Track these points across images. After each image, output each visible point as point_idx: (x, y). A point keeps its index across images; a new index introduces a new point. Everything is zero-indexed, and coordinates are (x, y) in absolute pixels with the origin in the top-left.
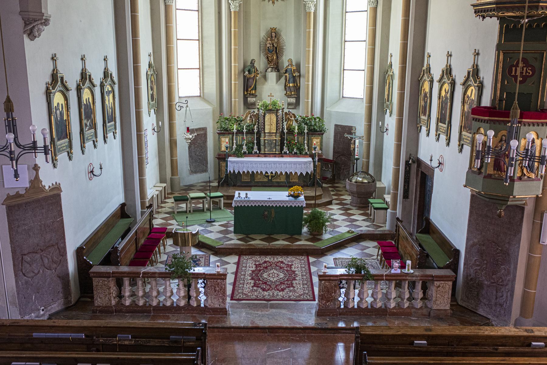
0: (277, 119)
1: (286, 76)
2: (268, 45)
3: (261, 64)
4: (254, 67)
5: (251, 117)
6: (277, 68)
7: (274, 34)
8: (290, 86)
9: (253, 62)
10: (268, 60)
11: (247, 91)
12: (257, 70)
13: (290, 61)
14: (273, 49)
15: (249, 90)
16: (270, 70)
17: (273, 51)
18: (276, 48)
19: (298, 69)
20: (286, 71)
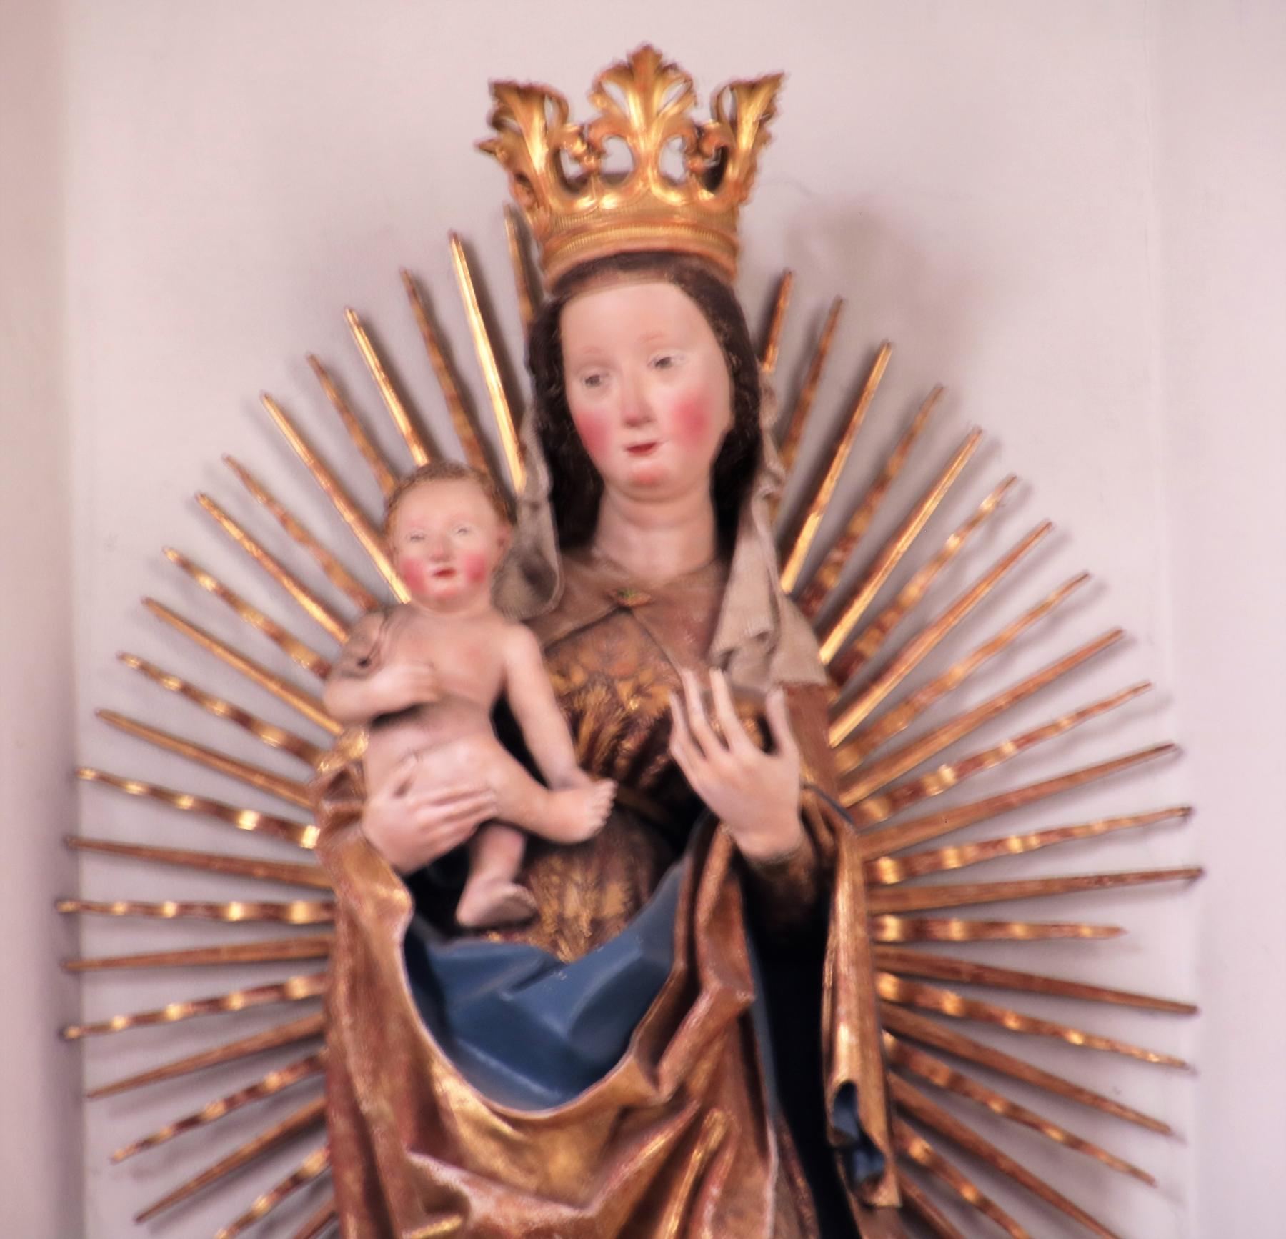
2: (433, 785)
7: (647, 373)
17: (646, 1003)
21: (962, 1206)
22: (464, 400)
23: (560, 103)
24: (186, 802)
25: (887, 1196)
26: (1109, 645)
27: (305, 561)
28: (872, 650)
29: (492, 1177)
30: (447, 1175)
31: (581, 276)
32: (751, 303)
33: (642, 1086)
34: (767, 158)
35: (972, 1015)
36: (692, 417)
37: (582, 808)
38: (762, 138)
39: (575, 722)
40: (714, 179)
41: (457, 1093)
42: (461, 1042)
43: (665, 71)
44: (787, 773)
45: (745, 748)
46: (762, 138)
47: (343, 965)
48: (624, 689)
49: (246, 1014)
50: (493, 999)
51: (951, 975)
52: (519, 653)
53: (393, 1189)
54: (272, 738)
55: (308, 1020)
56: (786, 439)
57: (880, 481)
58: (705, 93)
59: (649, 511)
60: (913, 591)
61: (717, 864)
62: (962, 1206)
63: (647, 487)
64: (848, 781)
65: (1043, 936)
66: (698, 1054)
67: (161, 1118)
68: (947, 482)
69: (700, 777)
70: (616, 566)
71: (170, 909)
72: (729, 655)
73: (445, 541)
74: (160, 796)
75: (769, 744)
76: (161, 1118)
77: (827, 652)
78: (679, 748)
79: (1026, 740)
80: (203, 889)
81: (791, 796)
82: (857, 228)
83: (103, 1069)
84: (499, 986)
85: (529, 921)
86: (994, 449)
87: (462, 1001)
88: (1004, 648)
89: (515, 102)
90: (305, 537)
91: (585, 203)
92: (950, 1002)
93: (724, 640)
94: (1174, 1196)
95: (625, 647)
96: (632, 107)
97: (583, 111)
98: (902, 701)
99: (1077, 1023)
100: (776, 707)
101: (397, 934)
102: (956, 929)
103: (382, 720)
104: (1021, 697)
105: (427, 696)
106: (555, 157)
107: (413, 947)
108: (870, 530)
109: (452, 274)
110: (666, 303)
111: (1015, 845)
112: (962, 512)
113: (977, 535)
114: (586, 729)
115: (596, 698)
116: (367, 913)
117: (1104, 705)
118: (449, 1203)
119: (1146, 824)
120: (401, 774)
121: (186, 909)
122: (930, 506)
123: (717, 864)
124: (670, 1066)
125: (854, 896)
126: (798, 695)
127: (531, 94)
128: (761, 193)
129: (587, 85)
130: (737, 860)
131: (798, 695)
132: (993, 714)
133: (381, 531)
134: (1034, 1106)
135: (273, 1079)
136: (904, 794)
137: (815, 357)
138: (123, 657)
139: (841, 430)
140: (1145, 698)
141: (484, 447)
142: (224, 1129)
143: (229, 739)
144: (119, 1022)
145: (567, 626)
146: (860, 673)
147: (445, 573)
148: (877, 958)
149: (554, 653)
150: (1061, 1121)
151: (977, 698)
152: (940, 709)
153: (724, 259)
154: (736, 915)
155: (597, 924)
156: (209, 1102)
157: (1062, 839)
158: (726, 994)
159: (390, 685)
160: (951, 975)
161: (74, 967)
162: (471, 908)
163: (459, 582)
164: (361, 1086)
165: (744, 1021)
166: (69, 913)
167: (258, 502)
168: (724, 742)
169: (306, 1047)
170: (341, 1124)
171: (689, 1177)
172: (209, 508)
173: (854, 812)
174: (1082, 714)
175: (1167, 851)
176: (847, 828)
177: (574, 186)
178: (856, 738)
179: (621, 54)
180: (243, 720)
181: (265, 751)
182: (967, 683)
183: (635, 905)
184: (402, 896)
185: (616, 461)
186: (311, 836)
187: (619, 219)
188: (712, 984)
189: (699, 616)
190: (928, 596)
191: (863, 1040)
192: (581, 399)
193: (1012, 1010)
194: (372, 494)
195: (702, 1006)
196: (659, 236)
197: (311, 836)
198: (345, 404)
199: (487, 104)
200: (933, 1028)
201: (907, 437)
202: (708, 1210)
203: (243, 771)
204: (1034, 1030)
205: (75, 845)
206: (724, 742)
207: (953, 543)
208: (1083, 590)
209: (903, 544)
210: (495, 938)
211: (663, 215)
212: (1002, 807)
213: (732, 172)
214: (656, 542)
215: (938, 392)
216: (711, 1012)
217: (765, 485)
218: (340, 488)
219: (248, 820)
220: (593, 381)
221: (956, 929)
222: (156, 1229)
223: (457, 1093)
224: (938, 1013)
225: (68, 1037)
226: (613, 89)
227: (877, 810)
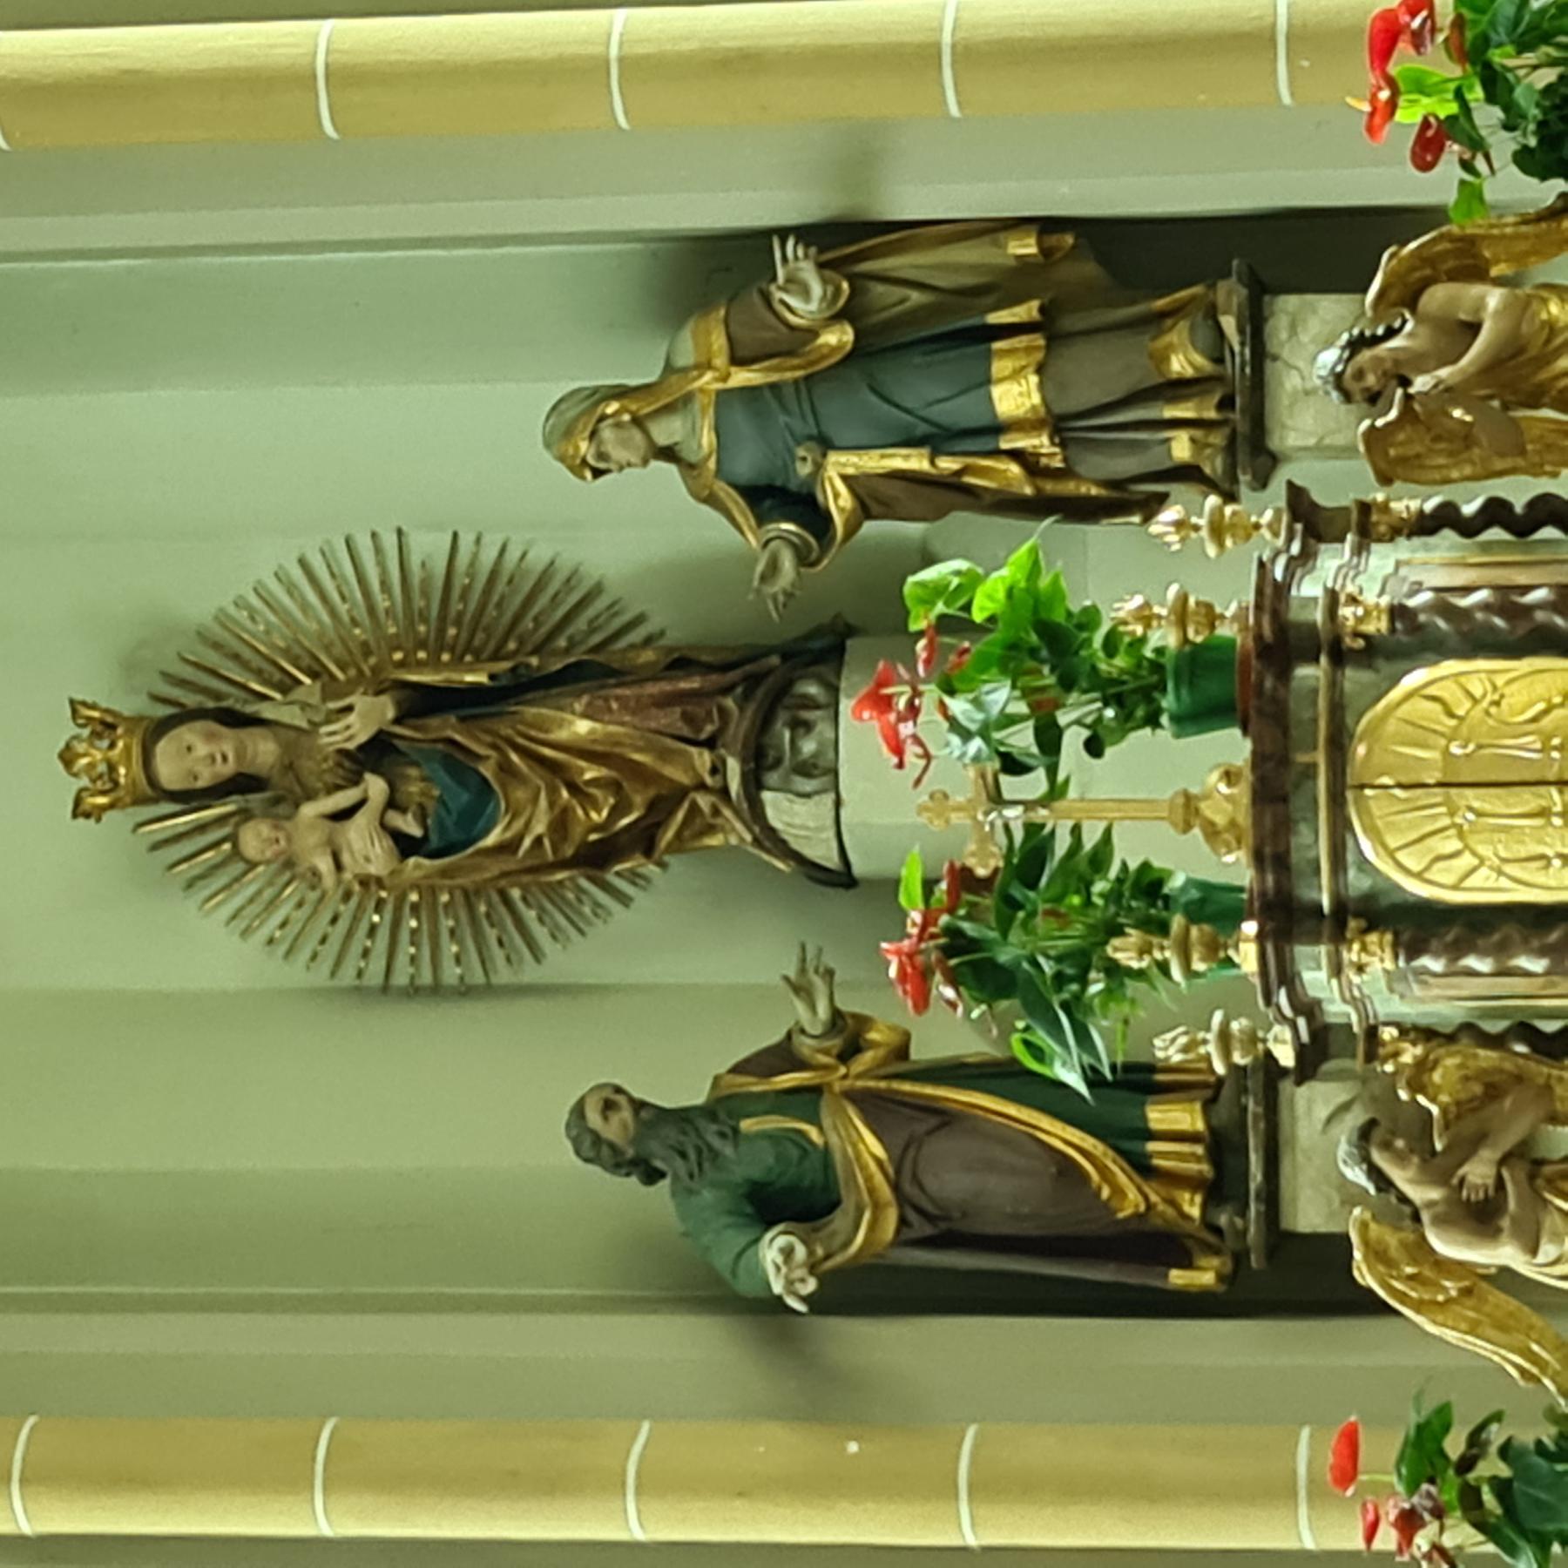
0: (1475, 641)
1: (873, 498)
2: (366, 847)
3: (680, 985)
4: (723, 1108)
5: (1481, 1216)
6: (763, 685)
7: (191, 756)
8: (1058, 424)
9: (636, 1140)
10: (644, 840)
11: (1171, 1246)
12: (782, 1056)
13: (588, 429)
14: (457, 752)
15: (1132, 1198)
16: (793, 814)
17: (457, 762)
18: (420, 703)
19: (718, 270)
20: (779, 497)
21: (536, 629)
22: (201, 828)
23: (81, 790)
24: (369, 943)
25: (534, 661)
26: (303, 563)
27: (268, 893)
28: (306, 661)
29: (527, 825)
30: (527, 842)
31: (152, 781)
32: (163, 711)
33: (492, 763)
34: (104, 705)
35: (458, 622)
36: (210, 737)
37: (375, 786)
38: (93, 707)
39: (338, 788)
40: (112, 727)
41: (491, 840)
42: (475, 832)
43: (68, 747)
44: (358, 700)
45: (352, 718)
46: (93, 707)
47: (438, 882)
48: (325, 766)
49: (457, 920)
50: (456, 824)
51: (441, 631)
52: (309, 810)
53: (529, 863)
54: (342, 908)
55: (458, 893)
56: (218, 696)
57: (236, 657)
58: (78, 731)
59: (249, 756)
60: (282, 644)
61: (398, 730)
62: (536, 629)
63: (240, 756)
64: (360, 672)
65: (425, 594)
66: (478, 741)
67: (498, 955)
68: (238, 630)
69: (362, 738)
70: (272, 767)
71: (412, 950)
72: (310, 722)
73: (264, 841)
74: (366, 953)
75: (349, 709)
76: (498, 955)
77: (307, 680)
78: (351, 746)
79: (343, 598)
80: (404, 936)
81: (369, 699)
82: (130, 666)
83: (478, 977)
84: (449, 822)
85: (422, 807)
86: (221, 610)
87: (455, 835)
88: (305, 607)
89: (81, 809)
90: (259, 893)
91: (122, 780)
92: (452, 631)
93: (304, 724)
94: (531, 543)
95: (307, 766)
96: (84, 761)
97: (84, 781)
98: (327, 648)
99: (460, 581)
100: (333, 705)
101: (426, 862)
102: (422, 628)
103: (339, 866)
104: (367, 594)
105: (329, 851)
106: (103, 793)
107: (432, 855)
108: (257, 662)
109: (150, 832)
110: (164, 750)
111: (387, 604)
112: (248, 624)
113: (258, 618)
114: (339, 782)
115: (329, 778)
116: (418, 874)
117: (329, 566)
118: (538, 841)
119: (378, 550)
120: (362, 861)
121: (413, 944)
122: (246, 636)
123: (398, 730)
124: (482, 751)
125: (410, 672)
126: (326, 696)
127: (78, 802)
128: (115, 707)
129: (73, 780)
130: (397, 721)
131: (326, 696)
132: (333, 613)
133: (252, 865)
134: (495, 598)
135: (483, 908)
136: (366, 650)
137: (183, 683)
138: (308, 968)
139: (214, 673)
140: (326, 549)
141: (221, 820)
142: (503, 929)
143: (343, 925)
144: (458, 971)
145: (297, 789)
146: (317, 668)
147: (277, 841)
148: (434, 664)
149: (310, 796)
150: (501, 587)
151: (326, 618)
152: (331, 634)
153: (145, 724)
154: (419, 722)
155: (424, 779)
156: (491, 934)
157: (385, 586)
158: (453, 728)
159: (324, 865)
160: (441, 631)
161: (436, 990)
162: (416, 831)
163: (281, 835)
164: (487, 875)
165: (462, 719)
166: (414, 991)
167: (244, 913)
168: (348, 727)
169: (469, 897)
170: (503, 883)
171: (533, 746)
172: (246, 933)
173: (374, 670)
174: (333, 575)
175: (390, 542)
176: (383, 676)
177: (116, 784)
178: (343, 668)
179: (60, 766)
180: (334, 920)
181: (346, 911)
182: (320, 622)
183: (416, 764)
184: (412, 861)
185: (228, 769)
186: (384, 894)
187: (128, 768)
188: (450, 733)
189: (292, 734)
190: (284, 638)
191: (471, 670)
192: (201, 784)
193: (456, 606)
194: (240, 867)
195: (458, 737)
196: (136, 751)
197: (384, 894)
198: (202, 877)
199: (81, 821)
200: (464, 635)
201: (217, 646)
202: (542, 736)
203: (356, 919)
204: (464, 597)
205: (385, 988)
206: (348, 727)
207: (262, 628)
208: (281, 574)
209: (262, 648)
210: (429, 821)
211: (127, 748)
212: (371, 609)
213: (109, 719)
214: (264, 751)
215: (199, 633)
216: (460, 733)
217: (238, 707)
218: (237, 880)
219: (376, 918)
220: (196, 778)
221: (422, 628)
222: (544, 955)
223: (491, 840)
224: (457, 636)
225: (465, 991)
226: (75, 769)
227: (373, 660)
